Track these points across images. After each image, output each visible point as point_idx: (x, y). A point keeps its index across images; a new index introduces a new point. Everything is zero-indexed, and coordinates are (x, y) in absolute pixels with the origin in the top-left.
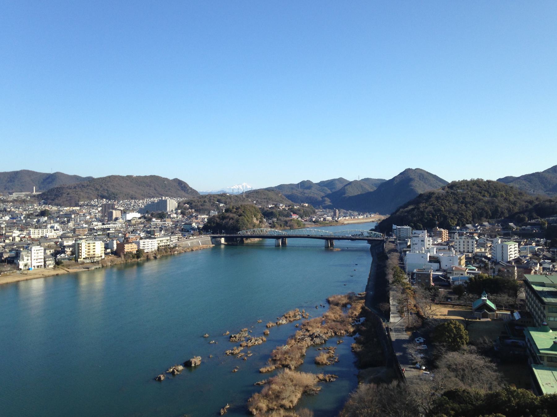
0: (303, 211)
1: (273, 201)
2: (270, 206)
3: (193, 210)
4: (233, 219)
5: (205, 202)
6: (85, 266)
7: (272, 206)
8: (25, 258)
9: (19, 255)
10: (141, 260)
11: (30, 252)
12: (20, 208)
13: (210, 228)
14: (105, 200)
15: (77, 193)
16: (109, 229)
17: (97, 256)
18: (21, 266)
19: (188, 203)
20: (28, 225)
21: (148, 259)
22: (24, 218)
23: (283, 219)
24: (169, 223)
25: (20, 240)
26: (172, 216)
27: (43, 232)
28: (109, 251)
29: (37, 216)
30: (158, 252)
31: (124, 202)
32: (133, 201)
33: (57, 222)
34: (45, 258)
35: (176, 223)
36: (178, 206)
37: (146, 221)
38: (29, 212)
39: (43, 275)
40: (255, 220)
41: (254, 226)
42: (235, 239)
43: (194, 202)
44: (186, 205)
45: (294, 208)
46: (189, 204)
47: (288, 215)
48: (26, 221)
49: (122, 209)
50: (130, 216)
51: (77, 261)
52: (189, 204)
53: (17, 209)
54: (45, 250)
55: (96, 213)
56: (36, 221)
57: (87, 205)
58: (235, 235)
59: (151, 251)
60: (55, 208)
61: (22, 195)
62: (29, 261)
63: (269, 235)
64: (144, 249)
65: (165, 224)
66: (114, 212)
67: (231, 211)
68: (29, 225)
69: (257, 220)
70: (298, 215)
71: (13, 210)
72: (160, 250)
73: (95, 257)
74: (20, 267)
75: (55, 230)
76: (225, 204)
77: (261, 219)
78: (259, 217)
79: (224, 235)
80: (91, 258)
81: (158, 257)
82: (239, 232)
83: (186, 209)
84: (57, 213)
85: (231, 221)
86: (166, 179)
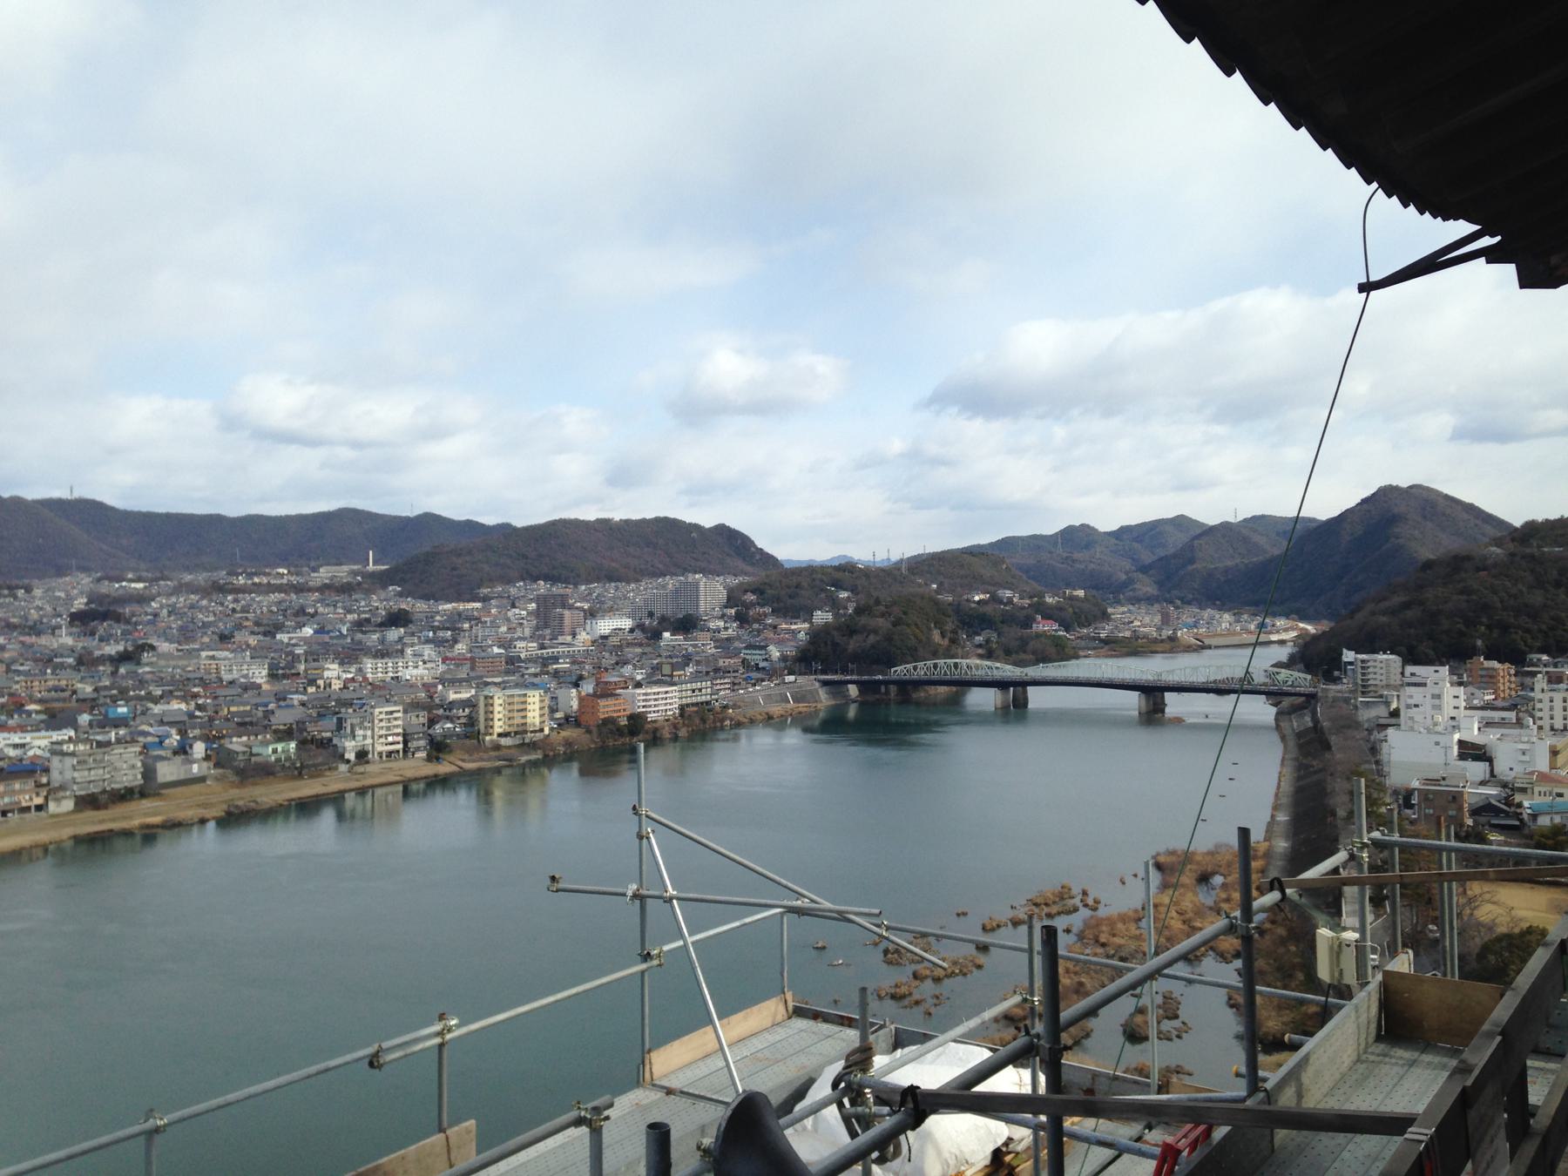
2: (977, 598)
3: (768, 610)
4: (875, 632)
7: (982, 597)
8: (359, 732)
9: (344, 725)
19: (753, 592)
23: (1014, 632)
28: (559, 715)
29: (381, 625)
31: (590, 589)
32: (613, 584)
33: (428, 641)
34: (405, 735)
36: (729, 599)
38: (359, 615)
40: (936, 636)
42: (883, 689)
43: (770, 586)
47: (1027, 623)
48: (352, 639)
50: (605, 626)
55: (523, 618)
61: (342, 572)
62: (369, 741)
68: (362, 650)
69: (943, 636)
72: (686, 715)
73: (525, 732)
77: (954, 632)
78: (949, 627)
79: (855, 677)
80: (516, 733)
81: (683, 733)
82: (893, 670)
85: (872, 639)
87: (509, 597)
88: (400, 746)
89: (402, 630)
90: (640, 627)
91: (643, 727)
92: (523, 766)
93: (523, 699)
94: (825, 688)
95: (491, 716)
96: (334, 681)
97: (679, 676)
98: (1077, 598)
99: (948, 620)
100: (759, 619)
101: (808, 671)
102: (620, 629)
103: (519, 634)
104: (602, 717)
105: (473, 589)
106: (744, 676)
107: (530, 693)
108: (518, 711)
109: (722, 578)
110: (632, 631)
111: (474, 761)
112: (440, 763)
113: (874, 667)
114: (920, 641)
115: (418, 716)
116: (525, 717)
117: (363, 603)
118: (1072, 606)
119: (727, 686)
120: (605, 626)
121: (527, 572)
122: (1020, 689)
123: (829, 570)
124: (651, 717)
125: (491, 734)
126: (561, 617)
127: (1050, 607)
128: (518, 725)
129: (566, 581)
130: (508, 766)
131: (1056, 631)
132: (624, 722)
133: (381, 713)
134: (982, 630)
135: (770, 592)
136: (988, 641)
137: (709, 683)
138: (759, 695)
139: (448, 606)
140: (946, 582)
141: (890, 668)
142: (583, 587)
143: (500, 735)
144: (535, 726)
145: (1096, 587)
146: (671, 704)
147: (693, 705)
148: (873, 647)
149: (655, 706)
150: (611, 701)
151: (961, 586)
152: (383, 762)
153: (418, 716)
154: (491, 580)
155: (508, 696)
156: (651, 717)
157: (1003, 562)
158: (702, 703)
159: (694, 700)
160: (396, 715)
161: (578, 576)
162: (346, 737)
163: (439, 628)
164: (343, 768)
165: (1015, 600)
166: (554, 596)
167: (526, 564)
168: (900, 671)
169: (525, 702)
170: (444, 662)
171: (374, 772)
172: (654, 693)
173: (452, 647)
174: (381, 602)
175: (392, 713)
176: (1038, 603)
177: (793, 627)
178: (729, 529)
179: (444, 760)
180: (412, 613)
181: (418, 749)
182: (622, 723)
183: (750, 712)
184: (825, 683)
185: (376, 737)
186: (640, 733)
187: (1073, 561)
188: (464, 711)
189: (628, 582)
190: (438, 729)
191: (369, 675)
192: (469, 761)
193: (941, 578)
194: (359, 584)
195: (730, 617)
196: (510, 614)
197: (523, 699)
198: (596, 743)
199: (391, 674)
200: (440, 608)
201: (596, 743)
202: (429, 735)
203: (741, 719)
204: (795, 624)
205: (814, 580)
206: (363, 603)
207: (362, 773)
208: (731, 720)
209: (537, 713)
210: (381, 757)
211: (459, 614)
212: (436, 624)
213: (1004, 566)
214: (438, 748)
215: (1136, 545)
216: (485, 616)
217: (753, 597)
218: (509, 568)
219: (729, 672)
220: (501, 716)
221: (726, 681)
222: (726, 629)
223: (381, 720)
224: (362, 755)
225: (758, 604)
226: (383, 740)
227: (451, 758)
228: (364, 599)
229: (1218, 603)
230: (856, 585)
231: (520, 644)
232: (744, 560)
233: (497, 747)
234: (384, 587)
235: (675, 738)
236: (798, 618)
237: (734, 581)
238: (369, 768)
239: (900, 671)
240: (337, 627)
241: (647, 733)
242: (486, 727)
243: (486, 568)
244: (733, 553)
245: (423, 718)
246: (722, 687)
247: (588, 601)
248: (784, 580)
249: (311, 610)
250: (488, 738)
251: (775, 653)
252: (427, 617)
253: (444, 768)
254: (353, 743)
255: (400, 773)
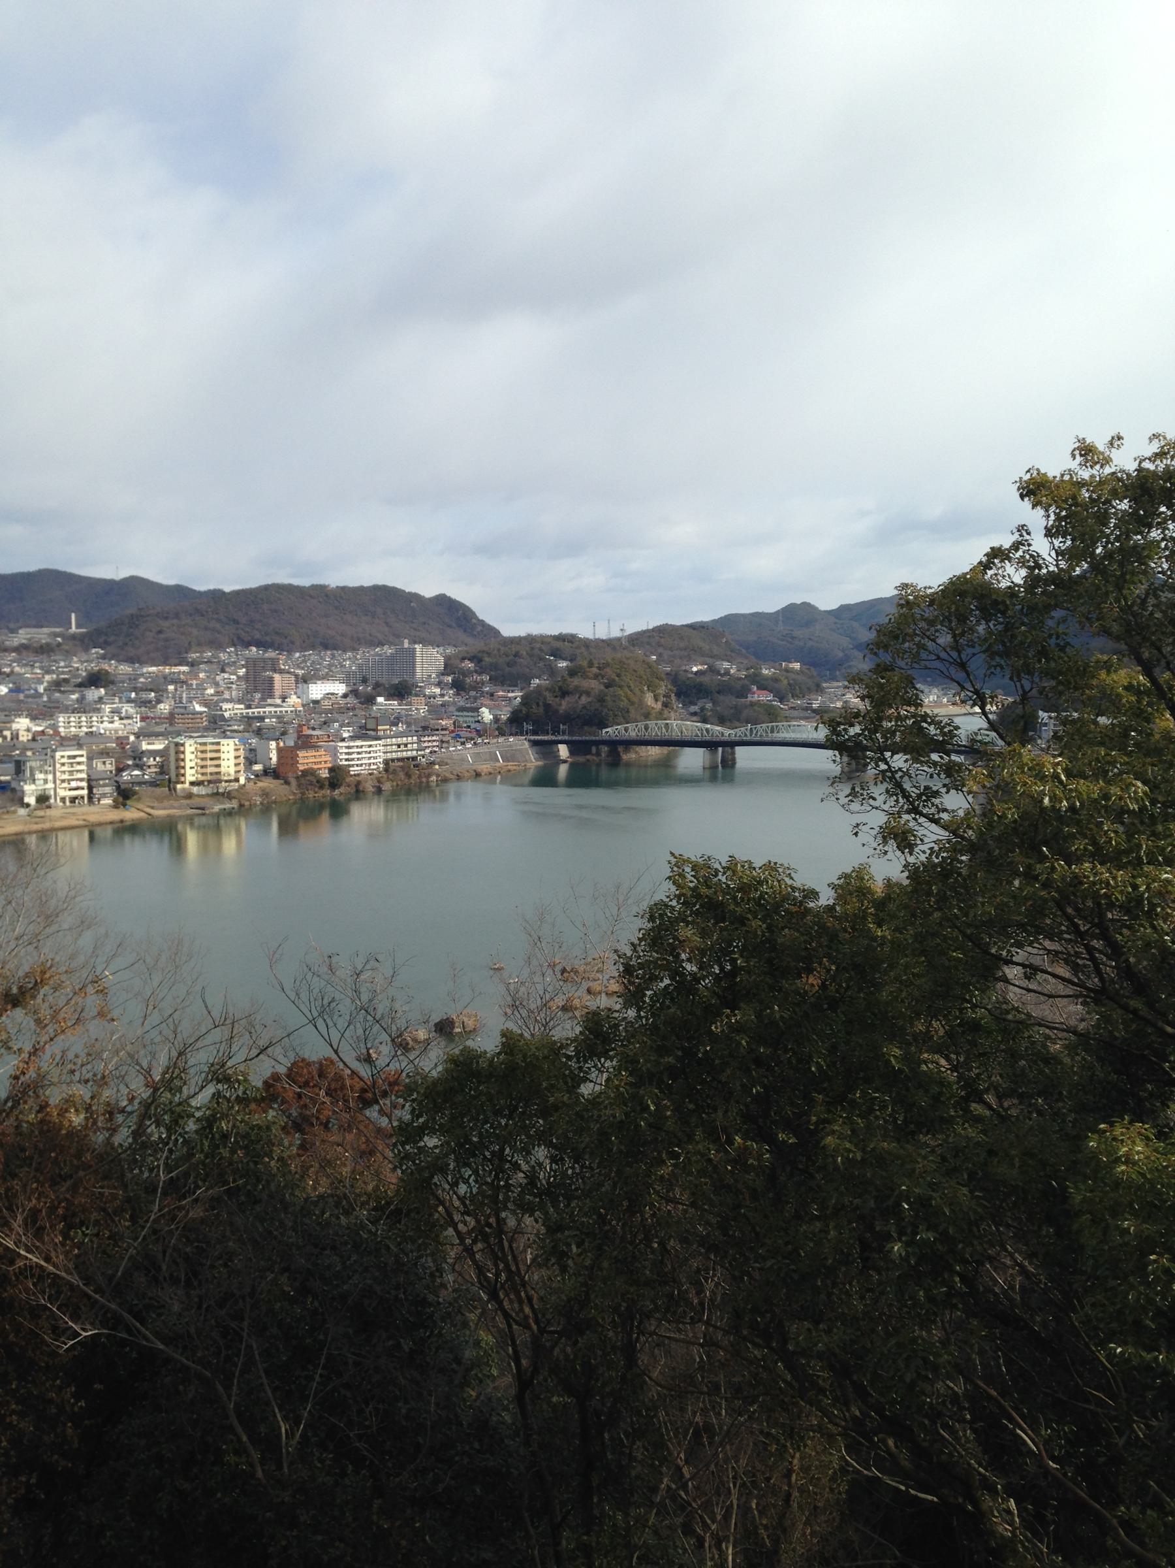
0: (785, 682)
1: (702, 656)
2: (695, 669)
3: (486, 678)
4: (588, 693)
5: (516, 655)
6: (196, 801)
7: (700, 667)
8: (40, 776)
9: (23, 768)
10: (341, 794)
11: (50, 761)
12: (37, 665)
13: (527, 718)
14: (254, 649)
15: (182, 630)
16: (261, 719)
17: (226, 778)
18: (31, 800)
19: (471, 660)
20: (54, 708)
21: (358, 793)
22: (45, 690)
23: (730, 700)
24: (419, 709)
25: (30, 738)
26: (427, 692)
27: (91, 722)
28: (258, 767)
29: (80, 685)
30: (385, 776)
31: (304, 656)
32: (329, 652)
33: (129, 701)
34: (89, 780)
35: (437, 711)
36: (446, 665)
37: (360, 703)
38: (58, 675)
39: (84, 820)
40: (649, 699)
41: (647, 716)
42: (594, 749)
43: (489, 654)
44: (467, 662)
45: (761, 674)
46: (475, 660)
47: (743, 692)
48: (49, 698)
49: (300, 672)
50: (317, 690)
51: (175, 789)
52: (475, 660)
53: (28, 669)
54: (90, 759)
55: (232, 683)
56: (77, 700)
57: (209, 662)
58: (594, 738)
59: (366, 772)
60: (125, 668)
61: (42, 635)
62: (50, 785)
63: (689, 738)
64: (350, 766)
65: (410, 710)
66: (277, 677)
67: (585, 676)
68: (58, 708)
69: (656, 699)
70: (771, 691)
71: (17, 669)
72: (391, 770)
73: (220, 781)
74: (26, 800)
75: (121, 719)
76: (571, 661)
77: (666, 696)
78: (662, 690)
79: (566, 738)
80: (210, 782)
81: (387, 786)
82: (604, 731)
83: (466, 673)
84: (130, 679)
85: (584, 700)
86: (415, 597)
87: (219, 662)
88: (85, 792)
89: (102, 691)
90: (354, 692)
91: (344, 779)
92: (218, 815)
93: (215, 747)
94: (535, 748)
95: (182, 756)
96: (21, 733)
97: (384, 730)
98: (792, 671)
99: (662, 683)
100: (476, 687)
101: (520, 732)
102: (332, 694)
103: (227, 696)
104: (301, 768)
105: (180, 653)
106: (453, 735)
107: (223, 741)
108: (211, 759)
109: (442, 648)
110: (345, 696)
111: (165, 809)
112: (127, 810)
113: (586, 728)
114: (632, 703)
115: (104, 763)
116: (219, 766)
117: (62, 664)
118: (787, 678)
119: (435, 744)
120: (317, 690)
121: (239, 638)
122: (728, 749)
123: (550, 640)
124: (354, 770)
125: (182, 783)
126: (271, 680)
127: (766, 678)
128: (211, 774)
129: (279, 648)
130: (198, 815)
131: (770, 701)
132: (325, 774)
133: (63, 757)
134: (698, 699)
135: (487, 659)
136: (702, 709)
137: (415, 738)
138: (466, 753)
139: (154, 669)
140: (666, 654)
141: (601, 729)
142: (297, 655)
143: (192, 784)
144: (229, 775)
145: (814, 664)
146: (375, 758)
147: (399, 760)
148: (584, 707)
149: (358, 759)
150: (311, 753)
151: (681, 658)
152: (67, 808)
153: (104, 763)
154: (199, 644)
155: (201, 744)
156: (354, 770)
157: (724, 636)
158: (408, 759)
159: (400, 755)
160: (79, 759)
161: (293, 643)
162: (25, 781)
163: (142, 690)
164: (22, 812)
165: (732, 671)
166: (264, 660)
167: (237, 629)
168: (610, 732)
169: (218, 751)
170: (143, 719)
171: (57, 814)
172: (357, 747)
173: (155, 707)
174: (81, 665)
175: (74, 757)
176: (755, 675)
177: (510, 695)
178: (450, 599)
179: (131, 806)
180: (115, 675)
181: (104, 795)
182: (324, 776)
183: (457, 770)
184: (535, 743)
185: (58, 782)
186: (341, 785)
187: (793, 638)
188: (155, 759)
189: (345, 651)
190: (126, 776)
191: (61, 730)
192: (158, 809)
193: (660, 650)
194: (59, 645)
195: (447, 684)
196: (218, 678)
197: (215, 747)
198: (294, 794)
199: (85, 729)
200: (145, 670)
201: (294, 794)
202: (117, 782)
203: (448, 775)
204: (513, 692)
205: (533, 649)
206: (62, 664)
207: (42, 817)
208: (438, 776)
209: (232, 762)
210: (64, 803)
211: (165, 677)
212: (139, 685)
213: (724, 640)
214: (124, 795)
215: (856, 625)
216: (191, 679)
217: (471, 665)
218: (219, 632)
219: (438, 730)
220: (193, 764)
221: (434, 738)
222: (442, 695)
223: (63, 764)
224: (43, 799)
225: (476, 671)
226: (65, 785)
227: (140, 806)
228: (64, 660)
229: (929, 679)
230: (575, 655)
231: (225, 706)
232: (465, 631)
233: (190, 796)
234: (86, 650)
235: (379, 791)
236: (516, 686)
237: (450, 651)
238: (49, 812)
239: (610, 732)
240: (33, 686)
241: (349, 786)
242: (177, 776)
243: (195, 632)
244: (454, 625)
245: (110, 766)
246: (430, 744)
247: (303, 669)
248: (502, 648)
249: (7, 670)
250: (179, 786)
251: (487, 715)
252: (130, 679)
253: (130, 814)
254: (33, 787)
255: (84, 817)
